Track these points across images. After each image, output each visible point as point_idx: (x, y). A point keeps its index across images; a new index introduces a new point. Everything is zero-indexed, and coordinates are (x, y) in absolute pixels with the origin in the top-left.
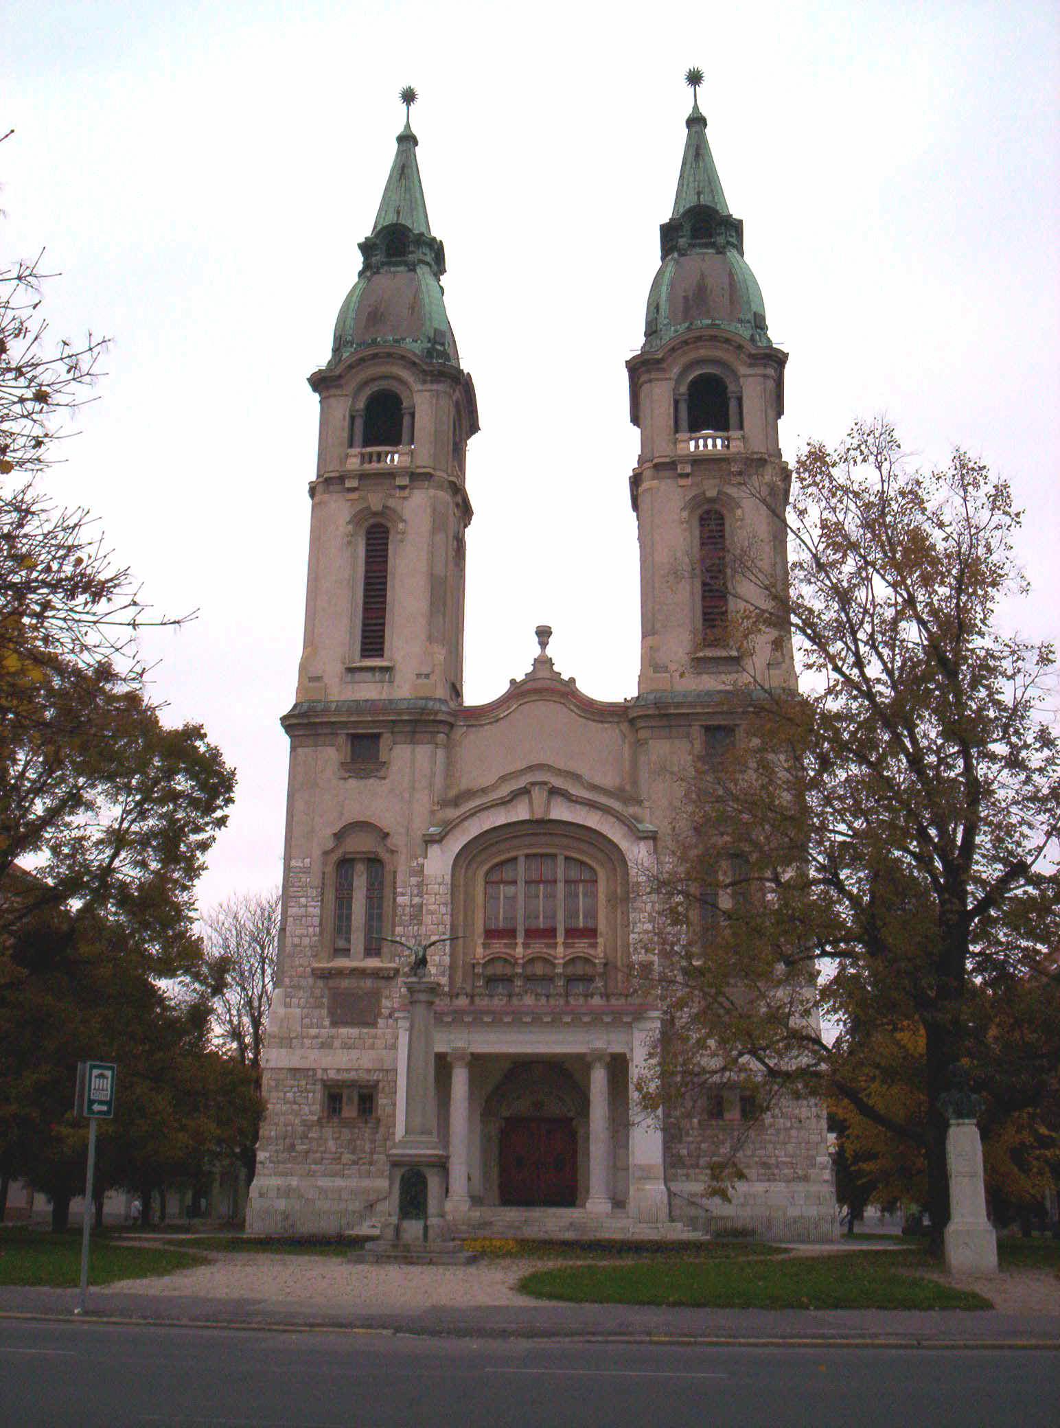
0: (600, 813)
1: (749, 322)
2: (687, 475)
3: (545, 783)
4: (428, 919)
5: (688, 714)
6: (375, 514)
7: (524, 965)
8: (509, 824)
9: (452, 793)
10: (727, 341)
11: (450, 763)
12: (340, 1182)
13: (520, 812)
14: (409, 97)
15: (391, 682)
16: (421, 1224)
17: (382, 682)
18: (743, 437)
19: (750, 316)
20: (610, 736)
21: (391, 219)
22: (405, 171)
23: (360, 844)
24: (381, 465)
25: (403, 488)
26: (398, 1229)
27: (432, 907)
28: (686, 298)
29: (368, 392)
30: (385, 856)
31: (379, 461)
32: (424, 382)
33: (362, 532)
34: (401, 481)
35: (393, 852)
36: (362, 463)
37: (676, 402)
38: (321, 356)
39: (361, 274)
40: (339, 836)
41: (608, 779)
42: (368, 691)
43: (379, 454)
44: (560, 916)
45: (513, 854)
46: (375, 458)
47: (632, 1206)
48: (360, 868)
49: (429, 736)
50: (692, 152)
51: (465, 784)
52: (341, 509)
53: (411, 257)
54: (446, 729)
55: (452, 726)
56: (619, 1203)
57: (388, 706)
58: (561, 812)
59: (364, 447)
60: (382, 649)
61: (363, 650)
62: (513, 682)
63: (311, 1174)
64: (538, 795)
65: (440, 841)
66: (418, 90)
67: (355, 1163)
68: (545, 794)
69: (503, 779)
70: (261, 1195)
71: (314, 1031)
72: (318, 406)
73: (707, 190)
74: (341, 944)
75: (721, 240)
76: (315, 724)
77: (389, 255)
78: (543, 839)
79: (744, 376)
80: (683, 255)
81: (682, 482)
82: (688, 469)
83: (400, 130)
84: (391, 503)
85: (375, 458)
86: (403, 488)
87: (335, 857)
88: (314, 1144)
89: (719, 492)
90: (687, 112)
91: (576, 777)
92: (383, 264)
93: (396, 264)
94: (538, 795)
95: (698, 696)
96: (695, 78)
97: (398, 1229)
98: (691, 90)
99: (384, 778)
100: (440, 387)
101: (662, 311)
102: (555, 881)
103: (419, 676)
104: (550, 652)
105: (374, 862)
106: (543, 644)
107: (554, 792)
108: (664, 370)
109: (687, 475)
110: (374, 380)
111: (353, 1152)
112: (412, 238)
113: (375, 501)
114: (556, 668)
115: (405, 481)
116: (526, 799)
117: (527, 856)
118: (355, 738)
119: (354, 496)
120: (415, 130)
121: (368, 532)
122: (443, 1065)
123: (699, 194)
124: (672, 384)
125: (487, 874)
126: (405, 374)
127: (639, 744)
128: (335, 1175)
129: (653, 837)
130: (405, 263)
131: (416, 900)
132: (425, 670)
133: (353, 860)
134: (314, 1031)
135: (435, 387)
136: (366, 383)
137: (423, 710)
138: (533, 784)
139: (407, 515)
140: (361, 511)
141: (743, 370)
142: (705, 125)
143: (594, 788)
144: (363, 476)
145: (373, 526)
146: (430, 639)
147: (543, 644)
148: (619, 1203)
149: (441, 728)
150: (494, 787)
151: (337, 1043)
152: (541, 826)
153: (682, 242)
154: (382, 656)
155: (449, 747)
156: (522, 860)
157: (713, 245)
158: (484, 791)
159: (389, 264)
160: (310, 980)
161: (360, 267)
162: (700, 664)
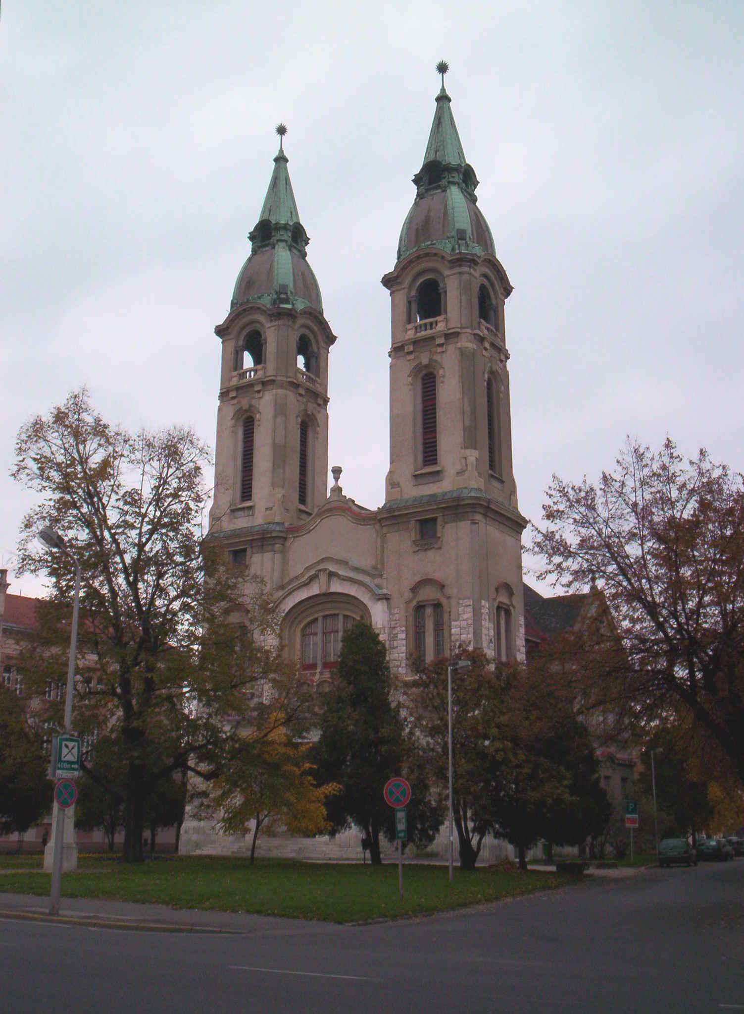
0: (357, 586)
1: (453, 237)
2: (411, 353)
3: (325, 570)
5: (407, 514)
6: (246, 411)
7: (318, 685)
8: (310, 598)
9: (286, 580)
10: (435, 255)
11: (285, 563)
13: (315, 590)
14: (443, 68)
15: (253, 515)
17: (248, 516)
18: (446, 318)
19: (454, 233)
20: (368, 533)
21: (432, 157)
22: (280, 183)
23: (428, 594)
24: (245, 380)
25: (259, 392)
28: (417, 230)
29: (244, 333)
30: (444, 601)
31: (431, 328)
32: (271, 321)
33: (241, 423)
34: (257, 388)
35: (449, 598)
36: (416, 332)
37: (409, 303)
38: (389, 265)
40: (414, 590)
41: (367, 562)
42: (242, 522)
43: (431, 324)
44: (319, 657)
45: (336, 612)
46: (428, 327)
48: (429, 611)
49: (270, 547)
51: (292, 575)
52: (407, 367)
54: (281, 541)
55: (285, 539)
57: (249, 531)
58: (337, 587)
60: (436, 459)
61: (243, 497)
64: (323, 577)
66: (446, 61)
68: (326, 576)
69: (307, 569)
70: (186, 832)
72: (221, 345)
75: (444, 182)
76: (395, 516)
77: (263, 241)
78: (329, 605)
79: (448, 276)
81: (409, 357)
82: (411, 348)
83: (276, 154)
84: (253, 402)
85: (428, 327)
86: (259, 392)
87: (414, 603)
89: (430, 360)
90: (437, 92)
91: (344, 563)
94: (323, 577)
95: (415, 501)
96: (282, 131)
98: (279, 136)
99: (440, 548)
100: (281, 322)
102: (337, 632)
103: (267, 509)
104: (341, 483)
105: (437, 606)
107: (332, 575)
108: (400, 283)
109: (411, 353)
110: (248, 325)
112: (273, 226)
113: (245, 403)
114: (343, 494)
115: (441, 340)
116: (317, 580)
117: (325, 617)
118: (423, 523)
119: (412, 357)
120: (449, 93)
121: (423, 379)
124: (406, 290)
125: (303, 630)
126: (262, 318)
127: (383, 537)
129: (386, 598)
132: (271, 505)
133: (424, 606)
135: (276, 323)
136: (244, 328)
137: (459, 499)
138: (320, 570)
139: (261, 409)
140: (417, 365)
141: (447, 272)
142: (450, 100)
143: (356, 569)
144: (415, 342)
145: (426, 375)
146: (273, 485)
149: (277, 541)
150: (302, 575)
152: (328, 597)
154: (436, 463)
155: (284, 552)
156: (320, 619)
158: (297, 578)
162: (417, 477)
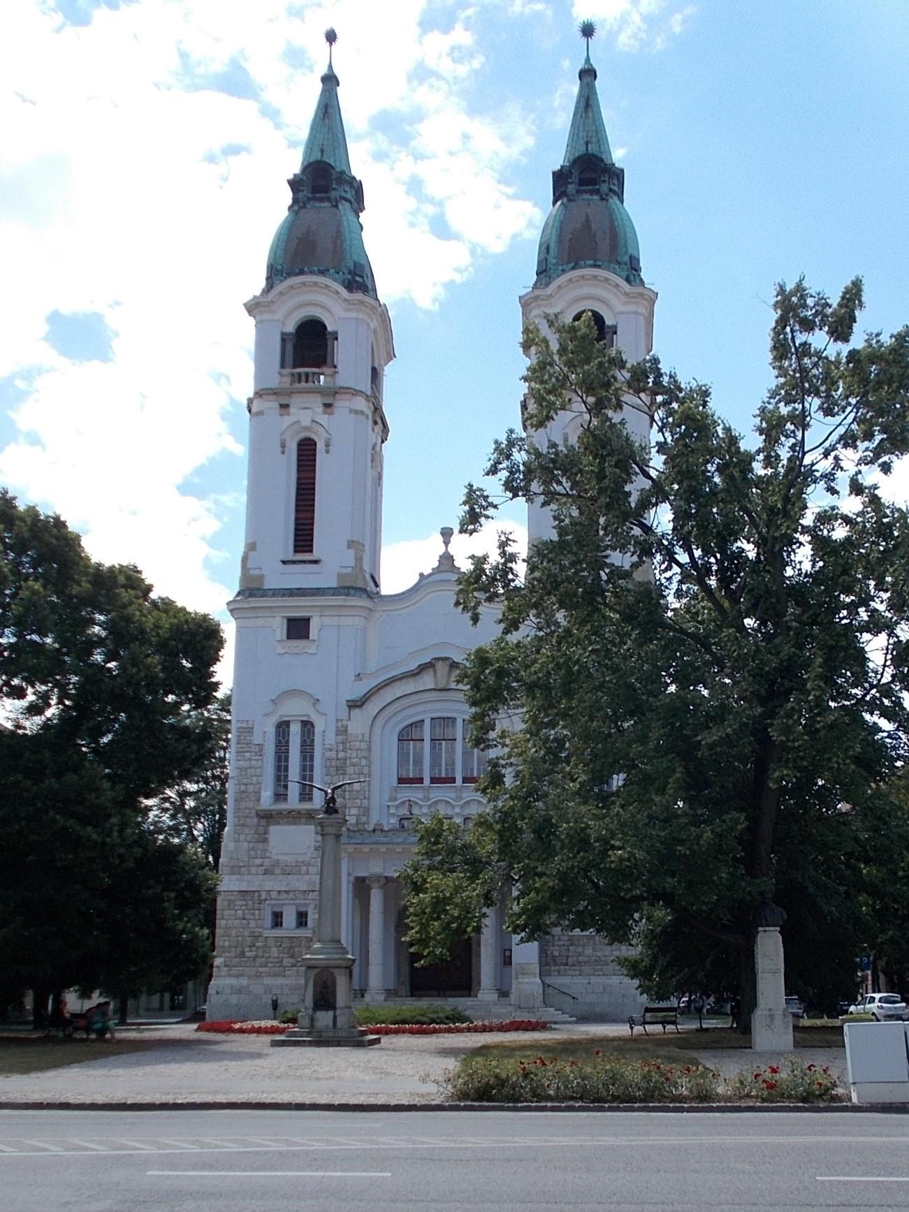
4: (350, 770)
12: (281, 981)
16: (331, 1013)
26: (312, 1020)
27: (355, 761)
32: (348, 310)
39: (290, 208)
46: (303, 378)
47: (513, 997)
50: (582, 104)
53: (333, 194)
56: (504, 993)
59: (294, 367)
62: (421, 575)
63: (258, 975)
65: (361, 706)
67: (293, 965)
71: (258, 861)
73: (594, 140)
74: (282, 791)
80: (570, 200)
85: (303, 378)
88: (260, 953)
92: (309, 199)
93: (321, 200)
97: (312, 1020)
101: (551, 251)
106: (447, 543)
111: (292, 957)
122: (361, 887)
123: (587, 144)
128: (276, 975)
130: (328, 199)
131: (341, 755)
134: (258, 861)
147: (447, 543)
148: (504, 993)
151: (277, 871)
153: (571, 189)
154: (286, 799)
157: (597, 192)
159: (315, 199)
160: (255, 820)
161: (290, 202)
